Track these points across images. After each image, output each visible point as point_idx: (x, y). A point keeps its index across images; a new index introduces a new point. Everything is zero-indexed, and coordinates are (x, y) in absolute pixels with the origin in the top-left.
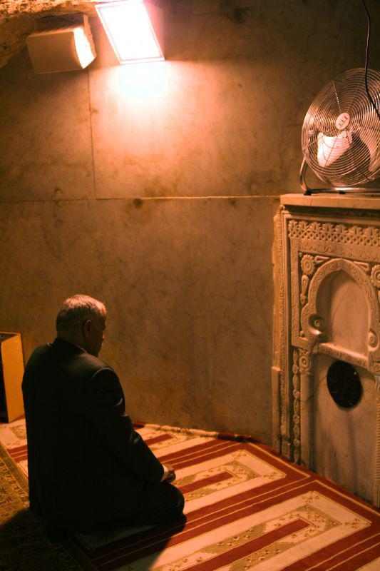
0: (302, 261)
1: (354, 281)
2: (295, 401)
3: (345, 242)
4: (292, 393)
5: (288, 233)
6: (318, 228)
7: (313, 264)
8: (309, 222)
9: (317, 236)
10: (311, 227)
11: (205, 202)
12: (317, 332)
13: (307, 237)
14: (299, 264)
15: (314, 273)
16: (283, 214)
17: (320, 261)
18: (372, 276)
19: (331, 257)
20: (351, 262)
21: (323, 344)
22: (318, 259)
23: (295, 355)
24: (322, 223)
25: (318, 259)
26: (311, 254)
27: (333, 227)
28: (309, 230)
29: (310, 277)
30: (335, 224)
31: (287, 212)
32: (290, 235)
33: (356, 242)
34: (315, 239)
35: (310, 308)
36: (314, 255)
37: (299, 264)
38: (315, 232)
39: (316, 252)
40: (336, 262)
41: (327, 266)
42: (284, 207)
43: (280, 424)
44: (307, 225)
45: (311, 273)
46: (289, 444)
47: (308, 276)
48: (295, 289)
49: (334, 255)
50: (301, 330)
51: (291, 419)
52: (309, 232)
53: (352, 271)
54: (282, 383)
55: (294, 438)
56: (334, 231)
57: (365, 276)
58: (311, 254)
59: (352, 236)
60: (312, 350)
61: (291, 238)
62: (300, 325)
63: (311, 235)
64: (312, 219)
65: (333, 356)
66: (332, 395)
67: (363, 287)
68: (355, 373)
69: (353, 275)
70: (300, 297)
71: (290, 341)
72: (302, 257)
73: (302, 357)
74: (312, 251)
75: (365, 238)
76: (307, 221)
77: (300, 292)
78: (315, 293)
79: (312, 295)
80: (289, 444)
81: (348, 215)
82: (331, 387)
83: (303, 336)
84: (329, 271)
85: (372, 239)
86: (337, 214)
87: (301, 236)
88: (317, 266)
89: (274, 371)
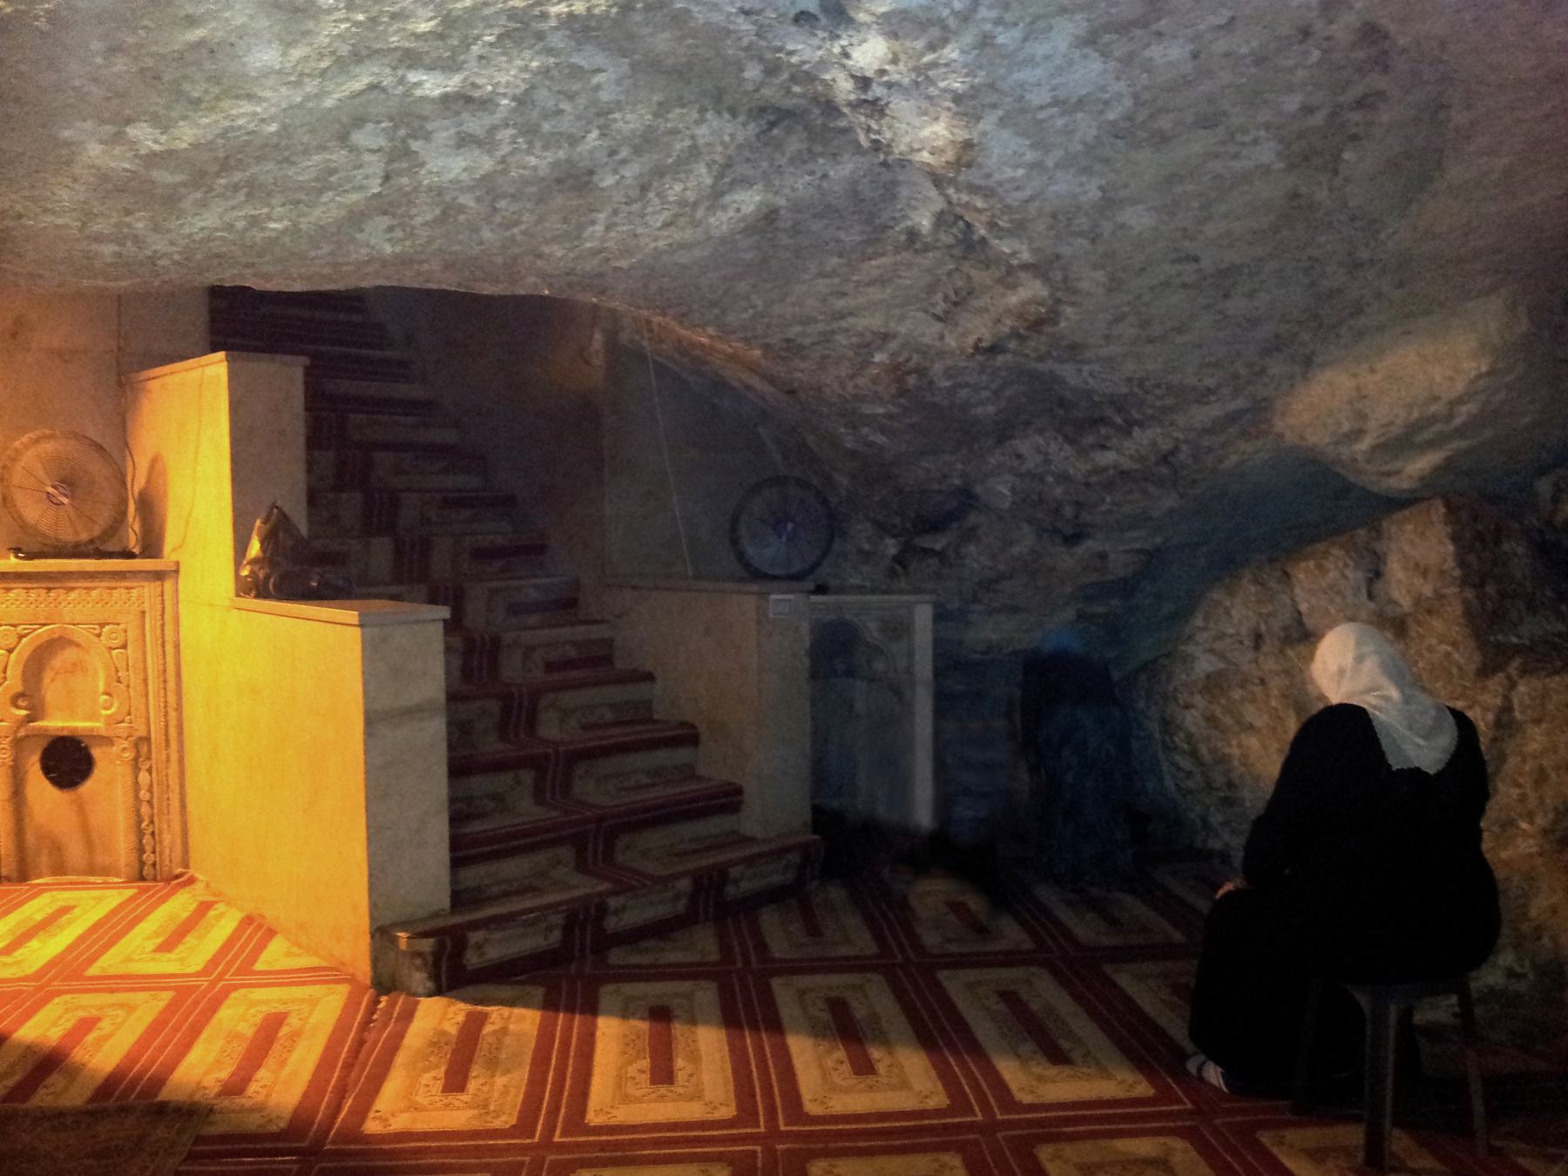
12: (23, 712)
30: (49, 589)
36: (14, 626)
82: (47, 770)
88: (21, 637)
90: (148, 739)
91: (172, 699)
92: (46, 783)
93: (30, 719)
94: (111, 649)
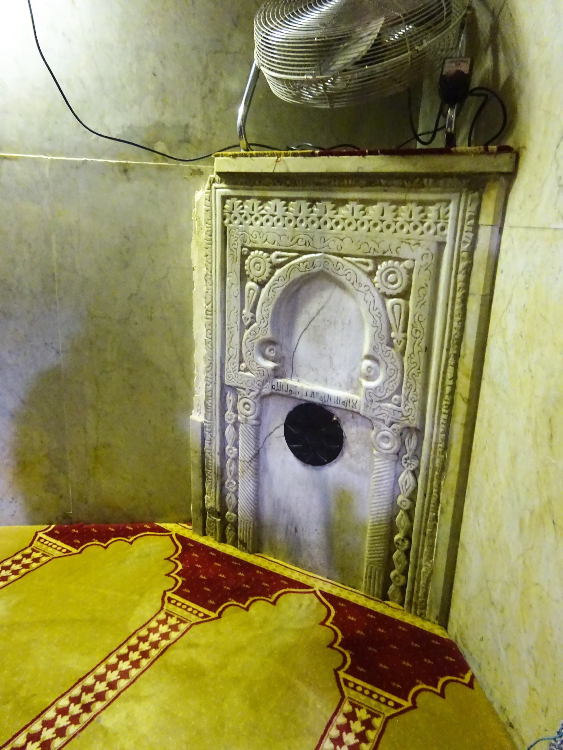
0: (247, 261)
1: (342, 286)
2: (228, 462)
3: (332, 228)
4: (224, 450)
5: (224, 218)
6: (389, 217)
7: (269, 265)
8: (264, 200)
9: (278, 220)
10: (269, 207)
11: (77, 166)
12: (270, 365)
13: (258, 223)
14: (243, 265)
15: (269, 279)
16: (216, 188)
17: (280, 260)
18: (376, 279)
19: (302, 253)
20: (339, 259)
21: (279, 380)
22: (278, 257)
23: (230, 397)
24: (287, 200)
25: (278, 257)
26: (265, 250)
27: (310, 206)
28: (263, 212)
29: (262, 285)
30: (313, 202)
31: (223, 185)
32: (227, 221)
33: (352, 228)
34: (273, 225)
35: (262, 328)
36: (269, 251)
37: (243, 265)
38: (274, 216)
39: (275, 246)
40: (313, 259)
41: (293, 267)
42: (218, 178)
43: (204, 493)
44: (260, 205)
45: (264, 278)
46: (219, 520)
47: (258, 283)
48: (233, 303)
49: (309, 249)
50: (241, 361)
51: (222, 485)
52: (263, 215)
53: (340, 272)
54: (208, 437)
55: (227, 511)
56: (312, 212)
57: (364, 279)
58: (265, 250)
59: (344, 219)
60: (261, 390)
61: (229, 227)
62: (241, 354)
63: (268, 220)
64: (270, 194)
65: (298, 396)
66: (292, 450)
67: (360, 296)
68: (335, 419)
69: (343, 279)
70: (241, 314)
71: (222, 378)
72: (249, 254)
73: (244, 400)
74: (267, 245)
75: (370, 221)
76: (259, 198)
77: (242, 307)
78: (271, 308)
79: (264, 312)
80: (219, 520)
81: (260, 183)
82: (291, 439)
83: (246, 370)
84: (296, 275)
85: (382, 221)
86: (318, 184)
87: (248, 222)
88: (275, 267)
89: (195, 421)
90: (419, 432)
91: (464, 385)
92: (291, 457)
93: (277, 373)
94: (385, 296)
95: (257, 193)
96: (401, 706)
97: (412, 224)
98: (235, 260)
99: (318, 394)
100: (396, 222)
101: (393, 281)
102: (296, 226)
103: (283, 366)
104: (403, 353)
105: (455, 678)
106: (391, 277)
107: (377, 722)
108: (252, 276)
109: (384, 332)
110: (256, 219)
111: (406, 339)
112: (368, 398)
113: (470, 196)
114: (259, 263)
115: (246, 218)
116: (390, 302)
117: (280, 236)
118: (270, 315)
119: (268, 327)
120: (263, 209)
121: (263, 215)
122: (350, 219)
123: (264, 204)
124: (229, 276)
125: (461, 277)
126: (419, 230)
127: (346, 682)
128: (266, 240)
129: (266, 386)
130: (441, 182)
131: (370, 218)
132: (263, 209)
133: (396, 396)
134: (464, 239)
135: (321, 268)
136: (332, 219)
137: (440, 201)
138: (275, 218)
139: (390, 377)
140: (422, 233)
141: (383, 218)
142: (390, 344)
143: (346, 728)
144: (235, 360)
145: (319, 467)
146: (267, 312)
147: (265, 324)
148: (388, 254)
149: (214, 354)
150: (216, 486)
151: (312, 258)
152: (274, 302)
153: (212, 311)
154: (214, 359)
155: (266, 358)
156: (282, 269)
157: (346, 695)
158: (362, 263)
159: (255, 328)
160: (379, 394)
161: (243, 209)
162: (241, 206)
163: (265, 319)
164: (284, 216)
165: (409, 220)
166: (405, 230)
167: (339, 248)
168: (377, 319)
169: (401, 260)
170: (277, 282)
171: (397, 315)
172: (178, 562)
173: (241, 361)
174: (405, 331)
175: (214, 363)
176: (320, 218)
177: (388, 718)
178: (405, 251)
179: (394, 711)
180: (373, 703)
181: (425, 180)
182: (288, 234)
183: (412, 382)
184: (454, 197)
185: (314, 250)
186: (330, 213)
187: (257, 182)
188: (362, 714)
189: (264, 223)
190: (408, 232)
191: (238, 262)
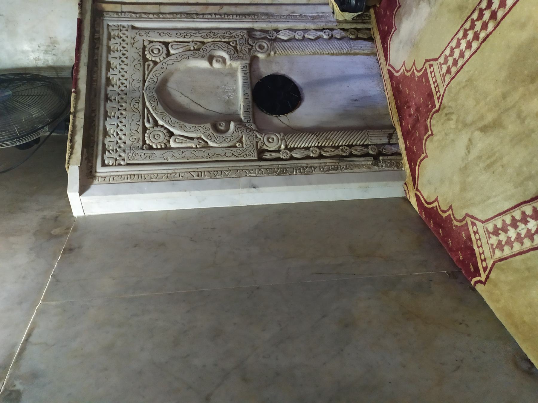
5: (120, 165)
7: (155, 128)
8: (106, 133)
9: (121, 122)
12: (232, 125)
15: (166, 128)
18: (158, 60)
24: (106, 116)
27: (111, 101)
28: (115, 134)
32: (122, 163)
36: (145, 129)
45: (165, 131)
47: (170, 137)
49: (141, 100)
52: (118, 134)
59: (119, 79)
64: (101, 128)
74: (140, 130)
75: (120, 65)
83: (240, 141)
85: (120, 58)
87: (122, 145)
88: (156, 124)
94: (168, 54)
95: (101, 138)
96: (472, 223)
97: (122, 42)
98: (154, 155)
99: (244, 91)
100: (121, 51)
101: (157, 50)
102: (125, 110)
103: (230, 117)
104: (203, 43)
105: (439, 209)
106: (156, 51)
107: (490, 227)
108: (165, 141)
109: (191, 52)
110: (120, 139)
111: (193, 41)
112: (237, 58)
113: (106, 16)
114: (154, 136)
115: (120, 147)
116: (172, 52)
117: (133, 120)
118: (193, 125)
119: (202, 126)
120: (113, 135)
121: (118, 134)
122: (119, 76)
123: (109, 134)
124: (167, 159)
125: (151, 16)
126: (125, 39)
127: (485, 269)
128: (136, 130)
129: (249, 127)
130: (97, 29)
131: (118, 65)
132: (113, 135)
133: (231, 43)
134: (129, 16)
135: (153, 91)
136: (119, 87)
137: (108, 29)
138: (120, 125)
139: (219, 47)
140: (127, 37)
141: (118, 58)
142: (198, 50)
143: (509, 242)
144: (235, 151)
145: (299, 89)
146: (191, 127)
147: (200, 128)
148: (141, 53)
149: (233, 168)
150: (351, 161)
151: (147, 97)
152: (182, 123)
153: (198, 172)
154: (238, 168)
155: (228, 129)
156: (157, 119)
157: (492, 262)
158: (148, 68)
159: (205, 136)
160: (232, 52)
161: (113, 150)
162: (111, 151)
163: (196, 129)
164: (118, 118)
165: (119, 44)
166: (125, 46)
167: (139, 81)
168: (183, 57)
169: (144, 47)
170: (167, 122)
171: (179, 47)
172: (421, 73)
173: (235, 146)
174: (189, 42)
175: (242, 168)
176: (119, 94)
177: (483, 222)
178: (139, 45)
179: (478, 223)
180: (484, 240)
181: (96, 37)
182: (131, 115)
183: (219, 35)
184: (105, 23)
185: (141, 97)
186: (116, 88)
187: (92, 138)
188: (494, 240)
189: (123, 132)
190: (127, 44)
191: (155, 152)
